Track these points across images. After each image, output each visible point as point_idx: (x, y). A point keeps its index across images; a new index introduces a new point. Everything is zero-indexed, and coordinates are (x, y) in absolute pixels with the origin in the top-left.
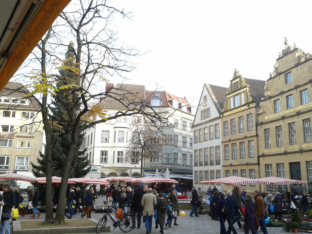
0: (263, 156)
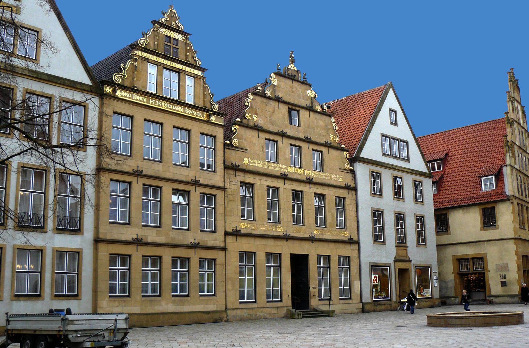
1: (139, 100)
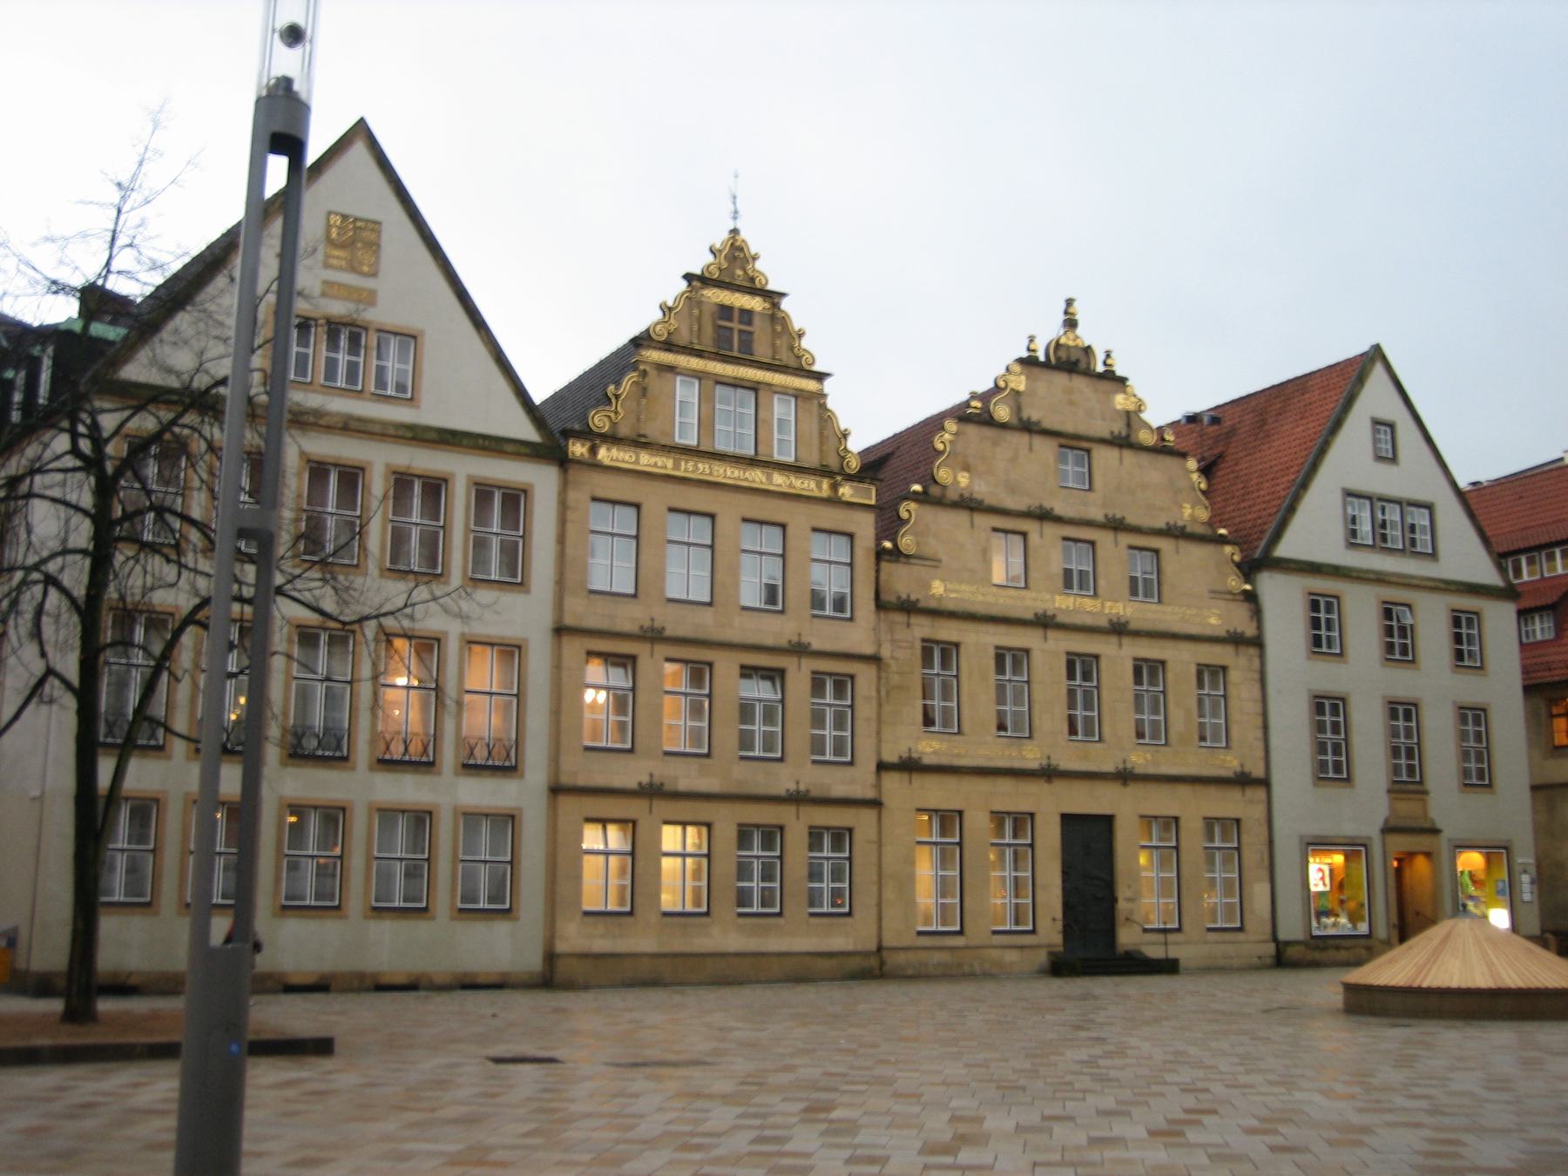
0: (910, 766)
1: (655, 465)
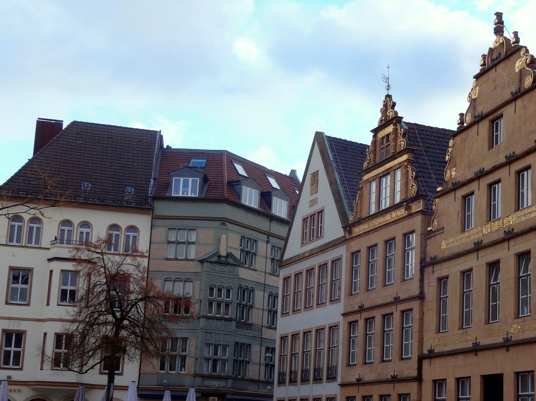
0: (432, 355)
